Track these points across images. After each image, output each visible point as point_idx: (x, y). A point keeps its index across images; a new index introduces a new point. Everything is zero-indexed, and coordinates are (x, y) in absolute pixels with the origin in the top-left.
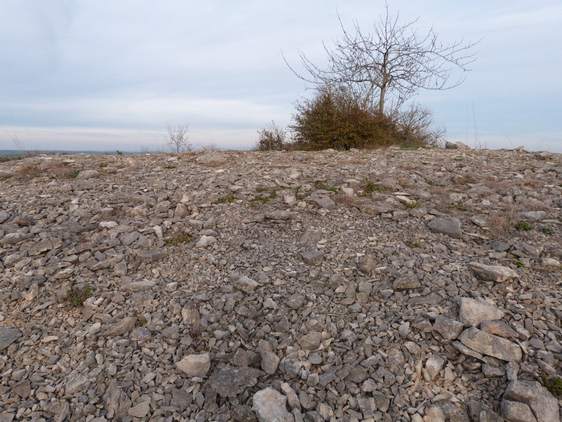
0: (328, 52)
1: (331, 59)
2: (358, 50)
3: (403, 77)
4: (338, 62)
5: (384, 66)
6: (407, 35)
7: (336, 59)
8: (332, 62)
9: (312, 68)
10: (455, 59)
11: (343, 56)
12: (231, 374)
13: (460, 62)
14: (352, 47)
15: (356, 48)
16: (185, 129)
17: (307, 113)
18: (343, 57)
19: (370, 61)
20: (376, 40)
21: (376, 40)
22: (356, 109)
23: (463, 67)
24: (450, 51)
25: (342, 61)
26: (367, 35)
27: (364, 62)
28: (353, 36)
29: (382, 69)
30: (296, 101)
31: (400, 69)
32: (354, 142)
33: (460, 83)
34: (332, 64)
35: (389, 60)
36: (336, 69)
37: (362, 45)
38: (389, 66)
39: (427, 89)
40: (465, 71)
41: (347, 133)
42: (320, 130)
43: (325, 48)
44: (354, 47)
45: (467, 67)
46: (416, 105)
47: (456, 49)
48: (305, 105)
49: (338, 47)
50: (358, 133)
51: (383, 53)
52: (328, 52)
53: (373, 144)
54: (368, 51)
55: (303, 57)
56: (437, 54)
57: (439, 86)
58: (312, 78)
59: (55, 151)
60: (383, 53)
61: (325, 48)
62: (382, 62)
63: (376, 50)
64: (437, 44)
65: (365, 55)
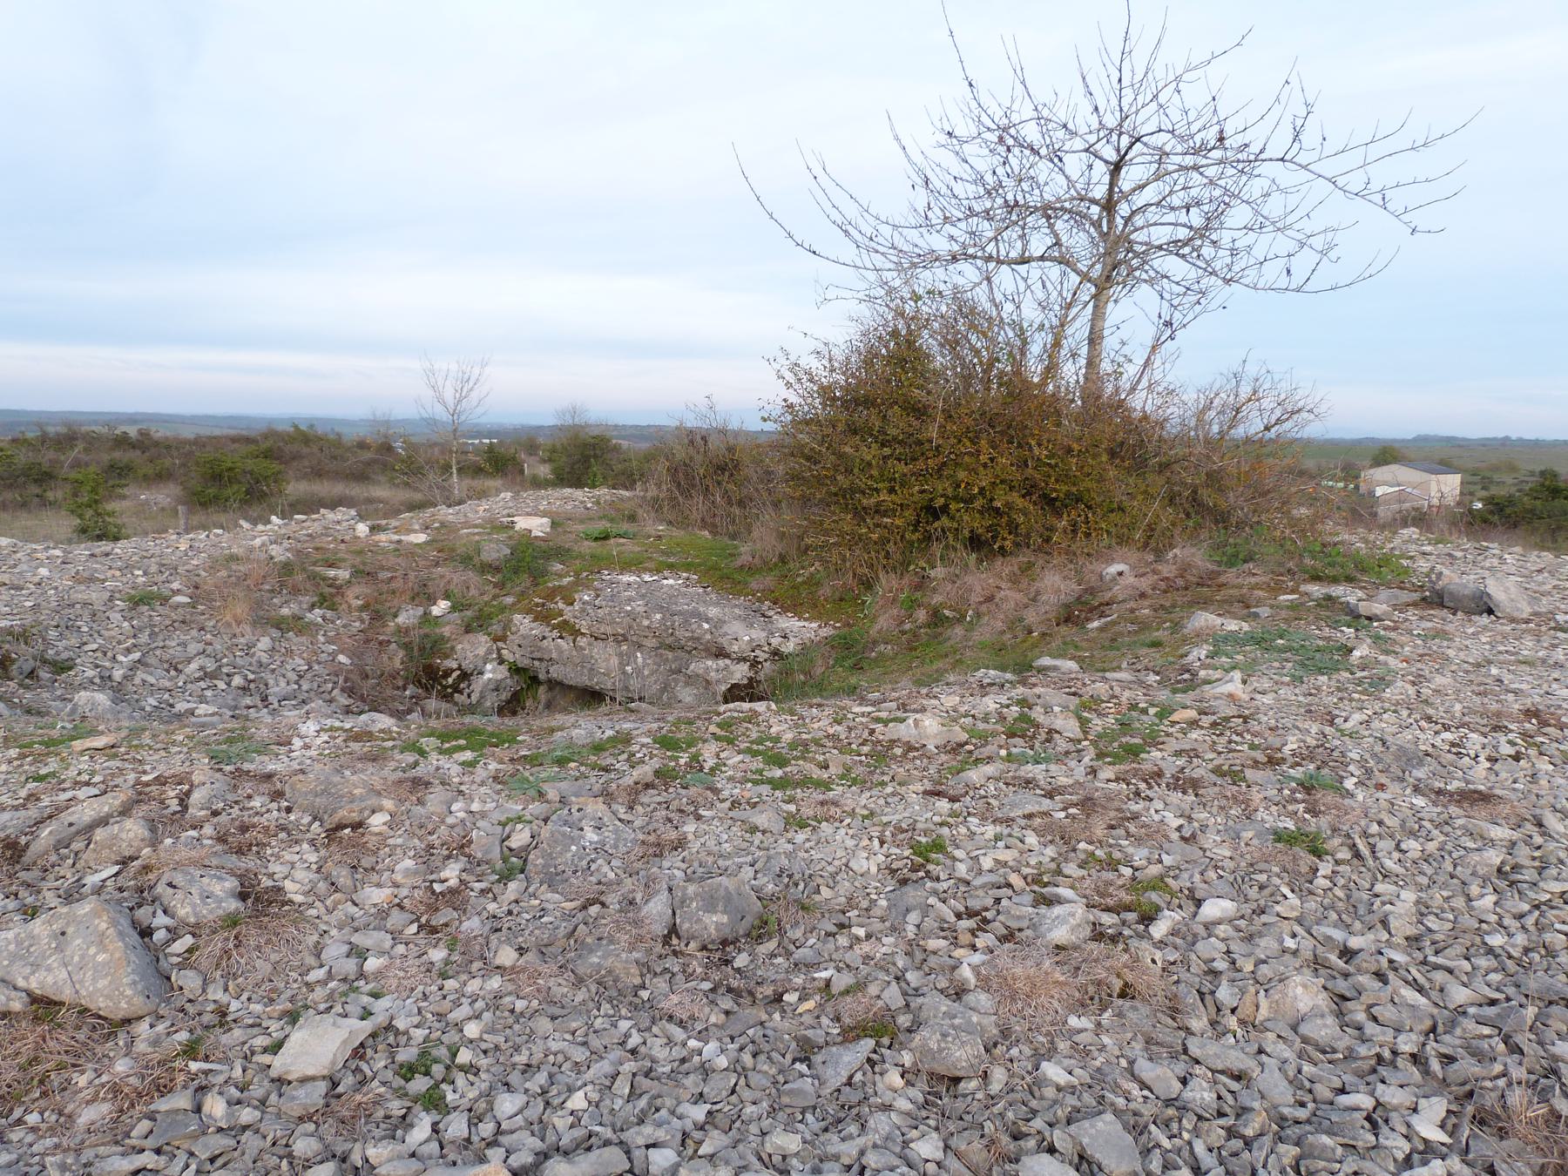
0: (907, 156)
1: (920, 181)
2: (1016, 150)
3: (1175, 247)
4: (944, 190)
5: (1109, 206)
6: (1195, 96)
7: (936, 183)
8: (921, 190)
9: (851, 211)
10: (1375, 186)
11: (957, 168)
12: (800, 423)
13: (1397, 200)
14: (993, 137)
15: (1010, 142)
16: (476, 371)
17: (826, 392)
18: (965, 176)
19: (1055, 188)
20: (1084, 119)
21: (1084, 119)
22: (1016, 387)
23: (1405, 218)
24: (1355, 158)
25: (959, 189)
26: (1048, 98)
27: (1037, 192)
28: (998, 95)
29: (1100, 219)
30: (780, 354)
31: (1166, 219)
32: (1013, 528)
33: (1371, 270)
34: (921, 198)
35: (1126, 186)
36: (936, 216)
37: (1031, 133)
38: (1124, 209)
39: (1255, 288)
40: (1417, 235)
41: (982, 490)
42: (875, 472)
43: (897, 139)
44: (1001, 139)
45: (1418, 218)
46: (1252, 370)
47: (1375, 151)
48: (816, 365)
49: (943, 138)
50: (1029, 489)
51: (1106, 162)
52: (907, 156)
53: (1088, 535)
54: (1056, 157)
55: (818, 171)
56: (1305, 167)
57: (1297, 280)
58: (848, 252)
59: (136, 414)
60: (1106, 162)
61: (897, 139)
62: (1099, 192)
63: (1087, 150)
64: (1310, 137)
65: (1043, 170)
